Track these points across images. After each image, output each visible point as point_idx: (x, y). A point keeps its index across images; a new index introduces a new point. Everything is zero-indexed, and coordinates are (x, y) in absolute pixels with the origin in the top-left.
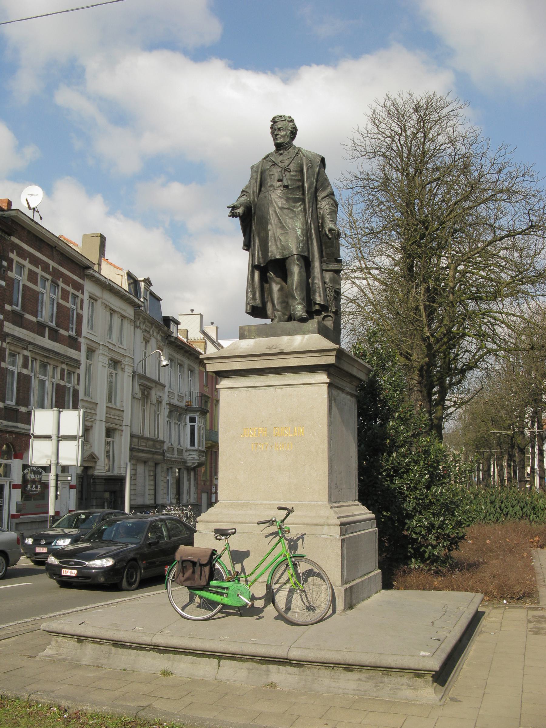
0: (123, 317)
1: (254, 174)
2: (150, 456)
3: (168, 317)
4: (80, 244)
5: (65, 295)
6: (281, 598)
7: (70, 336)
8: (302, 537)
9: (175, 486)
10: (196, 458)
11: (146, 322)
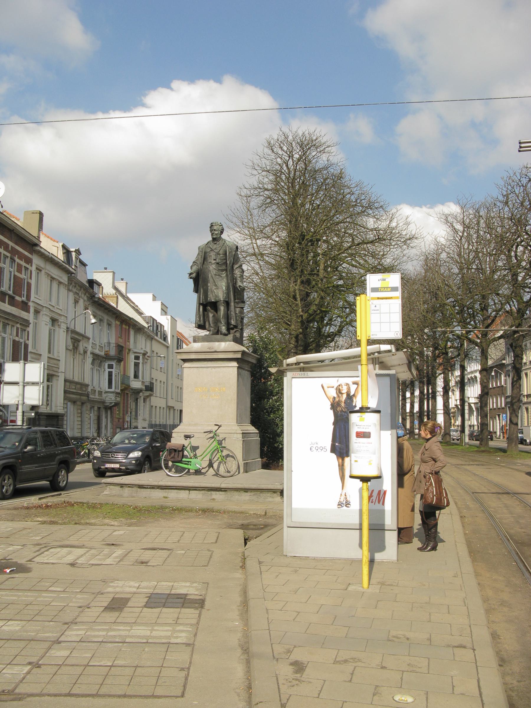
0: (60, 283)
1: (200, 253)
2: (78, 397)
3: (93, 280)
4: (22, 220)
5: (20, 268)
6: (215, 465)
7: (23, 301)
8: (225, 439)
9: (96, 422)
10: (113, 398)
11: (77, 286)
